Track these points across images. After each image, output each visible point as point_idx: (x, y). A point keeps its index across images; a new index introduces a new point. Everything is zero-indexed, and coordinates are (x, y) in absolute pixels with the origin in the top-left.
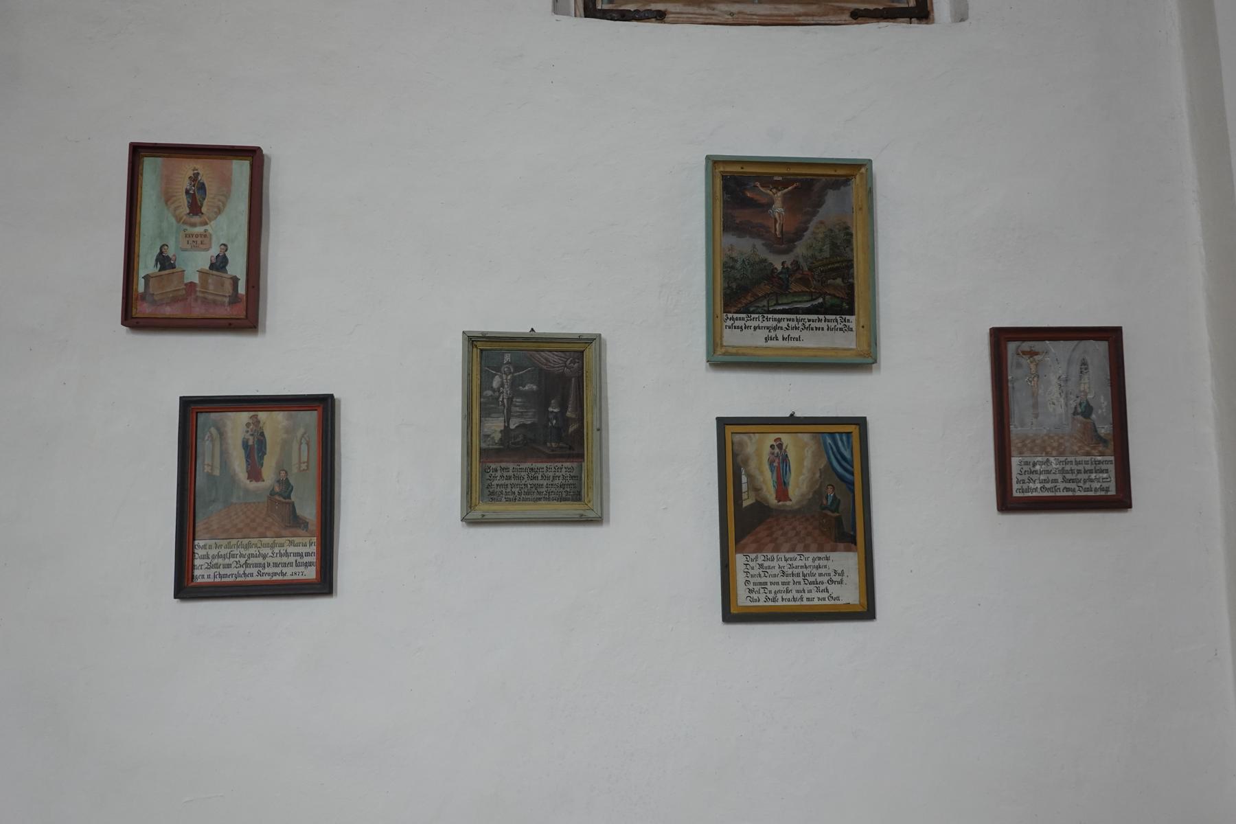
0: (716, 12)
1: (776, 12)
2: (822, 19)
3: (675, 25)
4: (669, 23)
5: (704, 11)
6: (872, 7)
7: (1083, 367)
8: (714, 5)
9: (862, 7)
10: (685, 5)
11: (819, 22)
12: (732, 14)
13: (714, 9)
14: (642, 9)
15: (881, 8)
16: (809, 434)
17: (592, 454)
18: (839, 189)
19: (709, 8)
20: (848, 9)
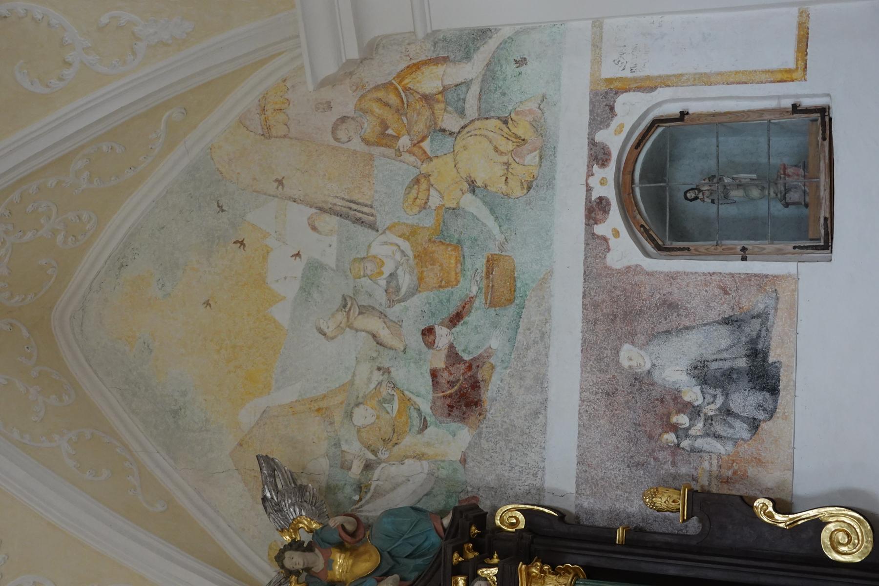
0: (824, 197)
1: (824, 172)
2: (824, 201)
3: (668, 261)
4: (748, 178)
5: (824, 201)
6: (821, 132)
7: (421, 456)
8: (821, 197)
9: (821, 136)
10: (821, 209)
11: (827, 161)
12: (825, 190)
13: (823, 198)
14: (823, 227)
15: (821, 128)
16: (796, 273)
17: (836, 514)
18: (777, 366)
19: (823, 200)
20: (822, 142)
